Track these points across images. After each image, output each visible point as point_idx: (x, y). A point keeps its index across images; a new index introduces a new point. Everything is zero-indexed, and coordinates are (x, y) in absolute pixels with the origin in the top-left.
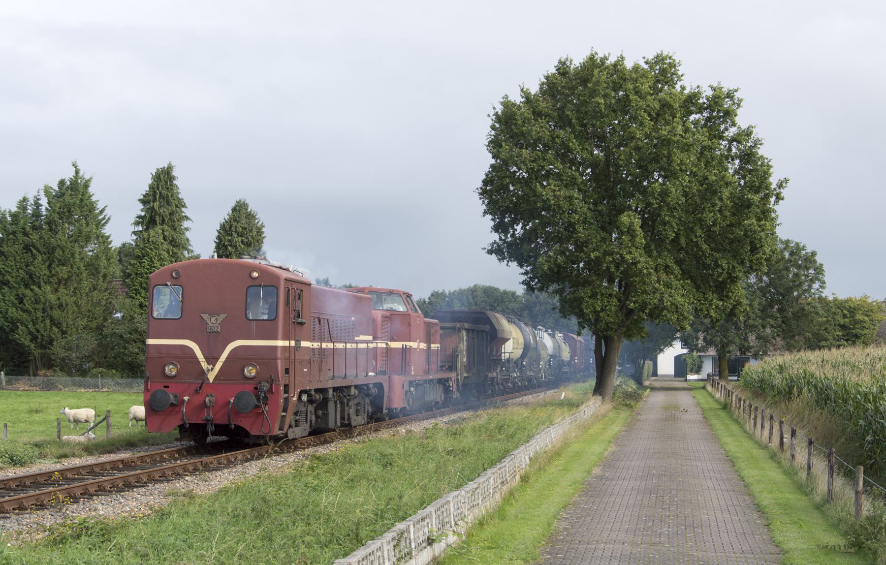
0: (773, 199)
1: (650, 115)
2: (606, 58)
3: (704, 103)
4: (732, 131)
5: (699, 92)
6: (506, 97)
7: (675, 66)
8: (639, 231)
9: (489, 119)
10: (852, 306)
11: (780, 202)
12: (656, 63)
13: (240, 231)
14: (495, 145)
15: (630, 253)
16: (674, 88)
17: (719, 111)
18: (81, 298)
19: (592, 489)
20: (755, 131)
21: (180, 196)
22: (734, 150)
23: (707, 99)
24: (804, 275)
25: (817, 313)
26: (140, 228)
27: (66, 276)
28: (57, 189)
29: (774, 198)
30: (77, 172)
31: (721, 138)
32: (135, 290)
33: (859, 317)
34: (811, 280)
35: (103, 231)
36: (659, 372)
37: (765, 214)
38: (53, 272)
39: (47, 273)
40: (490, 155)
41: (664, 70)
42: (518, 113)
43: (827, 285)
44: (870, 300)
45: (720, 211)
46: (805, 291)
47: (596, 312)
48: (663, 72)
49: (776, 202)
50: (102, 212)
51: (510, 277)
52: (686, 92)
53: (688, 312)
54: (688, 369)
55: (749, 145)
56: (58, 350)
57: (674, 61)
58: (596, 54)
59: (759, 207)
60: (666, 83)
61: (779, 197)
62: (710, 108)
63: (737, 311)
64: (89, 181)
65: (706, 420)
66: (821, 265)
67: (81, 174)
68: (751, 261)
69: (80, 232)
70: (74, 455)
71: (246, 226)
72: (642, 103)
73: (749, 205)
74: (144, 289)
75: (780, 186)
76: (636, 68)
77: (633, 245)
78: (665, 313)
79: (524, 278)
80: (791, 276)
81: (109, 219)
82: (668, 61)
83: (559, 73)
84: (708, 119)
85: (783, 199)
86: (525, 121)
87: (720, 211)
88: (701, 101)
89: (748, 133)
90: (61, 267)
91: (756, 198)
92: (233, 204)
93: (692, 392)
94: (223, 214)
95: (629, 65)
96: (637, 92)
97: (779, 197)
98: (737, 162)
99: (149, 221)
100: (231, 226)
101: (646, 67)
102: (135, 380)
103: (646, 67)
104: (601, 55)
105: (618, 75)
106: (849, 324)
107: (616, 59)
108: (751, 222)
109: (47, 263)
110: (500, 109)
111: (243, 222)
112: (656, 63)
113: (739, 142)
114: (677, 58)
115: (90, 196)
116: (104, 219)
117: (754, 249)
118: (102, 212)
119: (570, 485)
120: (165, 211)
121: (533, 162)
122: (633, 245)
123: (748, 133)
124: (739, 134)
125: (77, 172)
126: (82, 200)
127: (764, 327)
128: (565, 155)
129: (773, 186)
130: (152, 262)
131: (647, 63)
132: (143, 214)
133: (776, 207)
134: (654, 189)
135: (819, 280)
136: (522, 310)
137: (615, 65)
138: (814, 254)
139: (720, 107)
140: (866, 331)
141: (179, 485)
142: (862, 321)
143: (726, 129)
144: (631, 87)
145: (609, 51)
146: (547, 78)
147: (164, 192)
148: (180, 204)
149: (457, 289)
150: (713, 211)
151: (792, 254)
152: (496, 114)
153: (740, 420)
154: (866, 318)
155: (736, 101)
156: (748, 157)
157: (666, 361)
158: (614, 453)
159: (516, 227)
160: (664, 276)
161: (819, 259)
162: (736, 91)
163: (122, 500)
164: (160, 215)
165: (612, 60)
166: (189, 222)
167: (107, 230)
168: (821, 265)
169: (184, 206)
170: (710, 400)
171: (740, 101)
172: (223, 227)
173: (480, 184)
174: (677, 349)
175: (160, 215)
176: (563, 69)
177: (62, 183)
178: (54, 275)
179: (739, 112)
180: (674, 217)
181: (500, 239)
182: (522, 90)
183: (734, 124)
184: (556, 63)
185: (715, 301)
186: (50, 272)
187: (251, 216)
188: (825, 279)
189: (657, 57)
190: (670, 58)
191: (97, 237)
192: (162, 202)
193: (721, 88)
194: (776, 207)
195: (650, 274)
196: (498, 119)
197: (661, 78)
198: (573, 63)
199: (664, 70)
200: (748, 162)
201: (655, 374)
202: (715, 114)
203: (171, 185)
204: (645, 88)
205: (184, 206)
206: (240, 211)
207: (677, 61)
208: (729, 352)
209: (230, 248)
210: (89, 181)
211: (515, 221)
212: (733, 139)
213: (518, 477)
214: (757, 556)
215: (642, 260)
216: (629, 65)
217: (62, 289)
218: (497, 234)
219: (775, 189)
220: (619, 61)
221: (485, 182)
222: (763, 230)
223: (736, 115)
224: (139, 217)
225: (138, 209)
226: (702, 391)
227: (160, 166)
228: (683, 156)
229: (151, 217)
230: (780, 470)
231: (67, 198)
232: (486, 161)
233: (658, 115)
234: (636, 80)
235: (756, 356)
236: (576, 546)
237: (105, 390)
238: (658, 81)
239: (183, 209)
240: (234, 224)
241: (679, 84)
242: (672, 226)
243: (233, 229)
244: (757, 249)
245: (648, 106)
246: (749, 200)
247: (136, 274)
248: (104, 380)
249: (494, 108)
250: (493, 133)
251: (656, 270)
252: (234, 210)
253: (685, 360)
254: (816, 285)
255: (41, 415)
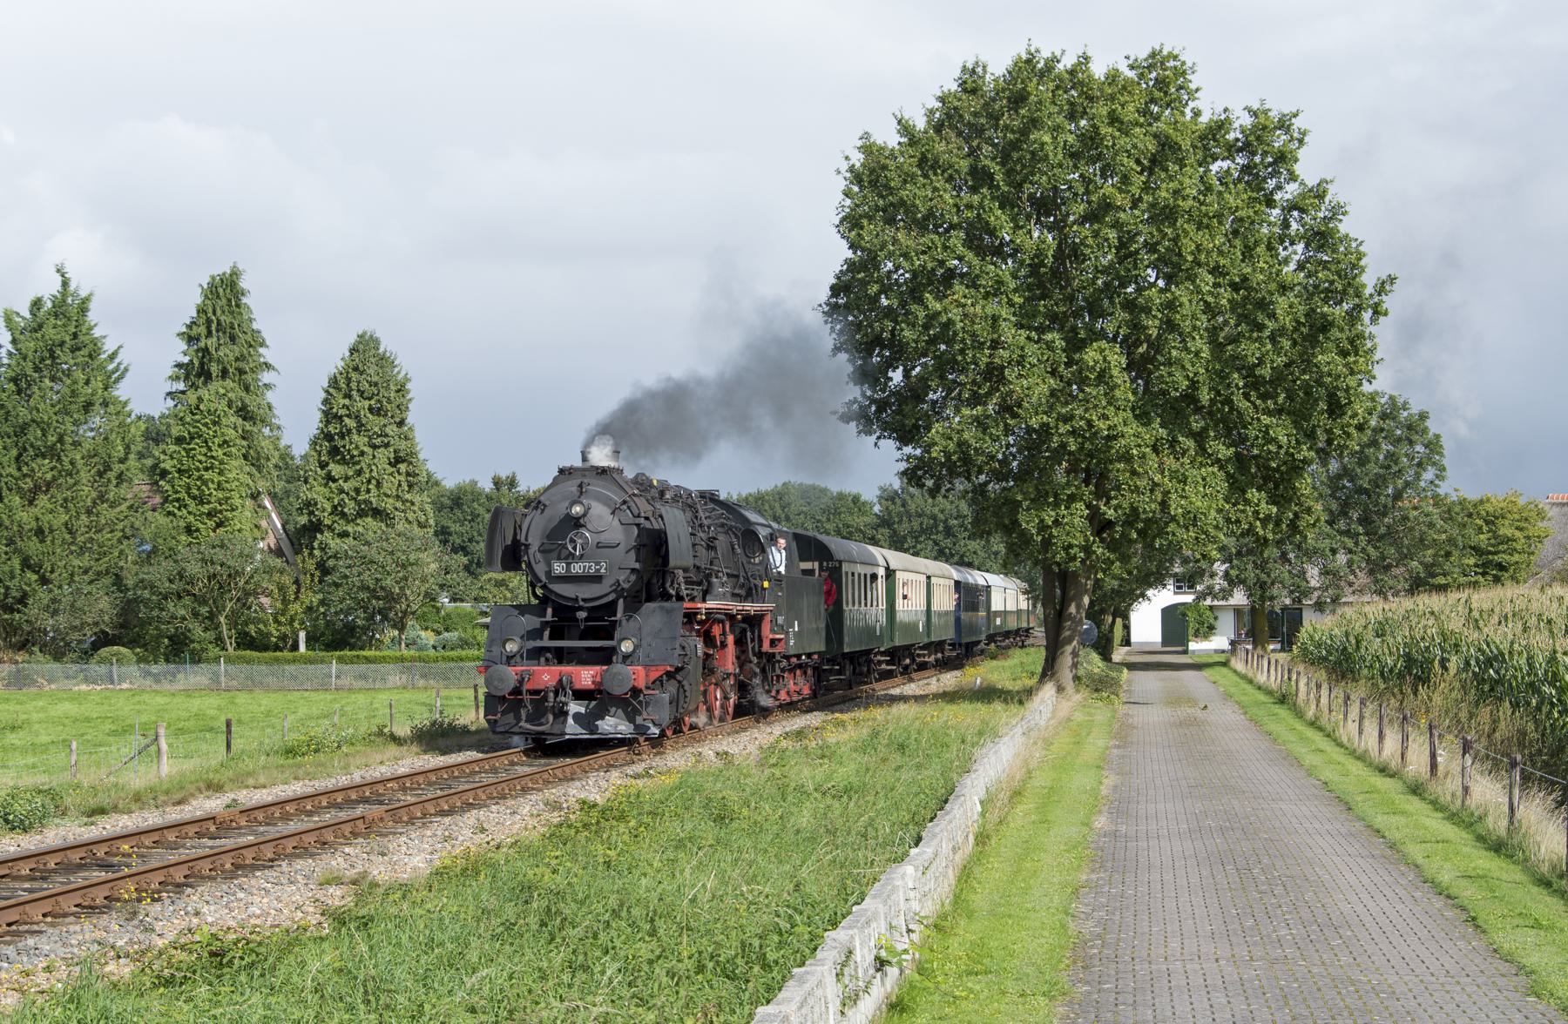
0: (1367, 316)
1: (1138, 162)
2: (1055, 60)
3: (1237, 140)
4: (1291, 190)
5: (1228, 118)
6: (866, 136)
7: (1184, 73)
8: (1119, 377)
9: (840, 177)
10: (1491, 510)
11: (1382, 318)
12: (1150, 67)
13: (366, 392)
14: (851, 223)
15: (1105, 417)
16: (1183, 113)
17: (1265, 153)
18: (78, 518)
19: (1109, 857)
20: (1332, 189)
21: (255, 326)
22: (1294, 226)
23: (1242, 132)
24: (1407, 455)
25: (1431, 525)
26: (181, 386)
27: (49, 476)
28: (28, 315)
29: (1370, 311)
30: (65, 284)
31: (1270, 203)
32: (178, 500)
33: (1506, 530)
34: (1420, 465)
35: (116, 393)
36: (1133, 639)
37: (1354, 347)
38: (25, 469)
39: (12, 470)
40: (844, 244)
41: (1163, 79)
42: (891, 164)
43: (1448, 473)
44: (1521, 502)
45: (1272, 338)
46: (1407, 484)
47: (1043, 527)
48: (1162, 84)
49: (1373, 321)
50: (112, 357)
51: (874, 468)
52: (1204, 119)
53: (1216, 527)
54: (1191, 631)
55: (1321, 215)
56: (35, 613)
57: (1184, 63)
58: (1038, 51)
59: (1342, 330)
60: (1168, 105)
61: (1377, 312)
62: (1247, 148)
63: (1302, 524)
64: (86, 300)
65: (1255, 721)
66: (1437, 436)
67: (72, 288)
68: (1329, 432)
69: (74, 393)
70: (115, 809)
71: (375, 379)
72: (1123, 141)
73: (1325, 326)
74: (194, 498)
75: (1381, 289)
76: (1113, 77)
77: (1110, 403)
78: (1172, 527)
79: (903, 466)
80: (1381, 457)
81: (126, 370)
82: (1172, 63)
83: (965, 91)
84: (1246, 169)
85: (1386, 314)
86: (908, 178)
87: (1272, 338)
88: (1231, 136)
89: (1319, 193)
90: (39, 460)
91: (1338, 312)
92: (352, 339)
93: (1207, 673)
94: (334, 358)
95: (1098, 70)
96: (1114, 119)
97: (1377, 312)
98: (1300, 247)
99: (197, 372)
100: (349, 380)
101: (1131, 74)
102: (181, 667)
103: (1131, 74)
104: (1046, 54)
105: (1076, 87)
106: (1489, 548)
107: (1074, 60)
108: (1326, 358)
109: (14, 452)
110: (857, 159)
111: (371, 371)
112: (1150, 67)
113: (1302, 211)
114: (1188, 58)
115: (91, 328)
116: (116, 370)
117: (1336, 408)
118: (112, 357)
119: (1068, 851)
120: (228, 353)
121: (924, 253)
122: (1110, 403)
123: (1319, 193)
124: (1303, 196)
125: (65, 284)
126: (75, 336)
127: (1334, 551)
128: (981, 239)
129: (1368, 291)
130: (210, 449)
131: (1132, 67)
132: (186, 360)
133: (1372, 329)
134: (1150, 299)
135: (1434, 464)
136: (876, 527)
137: (1072, 72)
138: (1423, 416)
139: (1265, 147)
140: (1516, 557)
141: (335, 862)
142: (1509, 540)
143: (1279, 187)
144: (1104, 111)
145: (1060, 44)
146: (942, 99)
147: (226, 319)
148: (257, 341)
149: (753, 490)
150: (1259, 339)
151: (1384, 416)
152: (851, 169)
153: (1324, 722)
154: (1518, 534)
155: (1296, 135)
156: (1321, 238)
157: (1146, 621)
158: (1116, 787)
159: (890, 374)
160: (1170, 462)
161: (1433, 426)
162: (1295, 116)
163: (241, 895)
164: (219, 361)
165: (1068, 62)
166: (272, 373)
167: (122, 391)
168: (1437, 436)
169: (263, 344)
170: (1249, 688)
171: (1304, 134)
172: (334, 382)
173: (824, 294)
174: (1164, 597)
175: (219, 361)
176: (971, 82)
177: (37, 304)
178: (25, 476)
179: (1301, 154)
180: (1187, 349)
181: (863, 394)
182: (899, 122)
183: (1293, 178)
184: (957, 73)
185: (1263, 505)
186: (19, 469)
187: (384, 361)
188: (1445, 462)
189: (1153, 55)
190: (1175, 58)
191: (105, 404)
192: (221, 335)
193: (1266, 112)
194: (1372, 329)
195: (1143, 456)
196: (857, 177)
197: (1157, 94)
198: (989, 69)
199: (1163, 79)
200: (1320, 248)
201: (1127, 642)
202: (1257, 159)
203: (238, 306)
204: (1129, 113)
205: (263, 344)
206: (365, 350)
207: (1189, 64)
208: (1272, 598)
209: (347, 420)
210: (86, 300)
211: (890, 364)
212: (1293, 206)
213: (971, 838)
214: (1480, 981)
215: (1129, 430)
216: (1098, 70)
217: (43, 500)
218: (857, 388)
219: (1371, 296)
220: (1080, 63)
221: (835, 290)
222: (1352, 373)
223: (1296, 160)
224: (179, 366)
225: (178, 351)
226: (1224, 670)
227: (218, 271)
228: (1202, 237)
229: (202, 364)
230: (1440, 815)
231: (49, 332)
232: (837, 254)
233: (1153, 161)
234: (1112, 98)
235: (1319, 606)
236: (1130, 967)
237: (125, 686)
238: (1153, 101)
239: (261, 350)
240: (354, 376)
241: (1191, 104)
242: (1183, 367)
243: (354, 385)
244: (1341, 407)
245: (1135, 146)
246: (1324, 315)
247: (179, 471)
248: (123, 669)
249: (847, 158)
250: (848, 202)
251: (1155, 449)
252: (353, 350)
253: (1184, 615)
254: (1429, 474)
255: (21, 733)
